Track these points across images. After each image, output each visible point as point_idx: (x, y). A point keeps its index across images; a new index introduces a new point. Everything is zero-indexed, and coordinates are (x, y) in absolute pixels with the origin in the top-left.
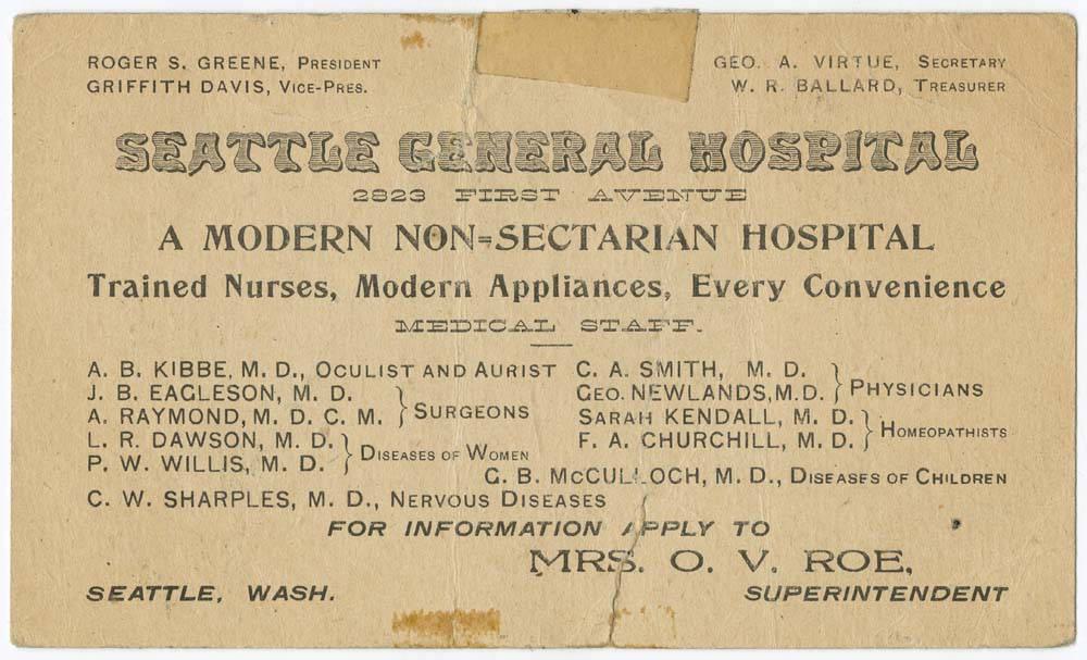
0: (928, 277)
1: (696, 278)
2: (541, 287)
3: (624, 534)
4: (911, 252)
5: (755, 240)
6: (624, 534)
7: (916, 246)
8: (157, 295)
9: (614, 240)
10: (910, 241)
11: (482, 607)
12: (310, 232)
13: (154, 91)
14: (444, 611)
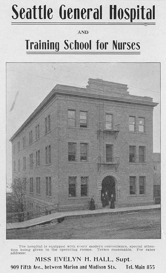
0: (40, 41)
1: (55, 258)
2: (125, 260)
3: (74, 261)
4: (103, 262)
5: (96, 260)
6: (74, 261)
7: (104, 261)
8: (122, 259)
9: (101, 260)
10: (103, 260)
11: (144, 117)
12: (66, 258)
13: (108, 258)
14: (76, 191)
